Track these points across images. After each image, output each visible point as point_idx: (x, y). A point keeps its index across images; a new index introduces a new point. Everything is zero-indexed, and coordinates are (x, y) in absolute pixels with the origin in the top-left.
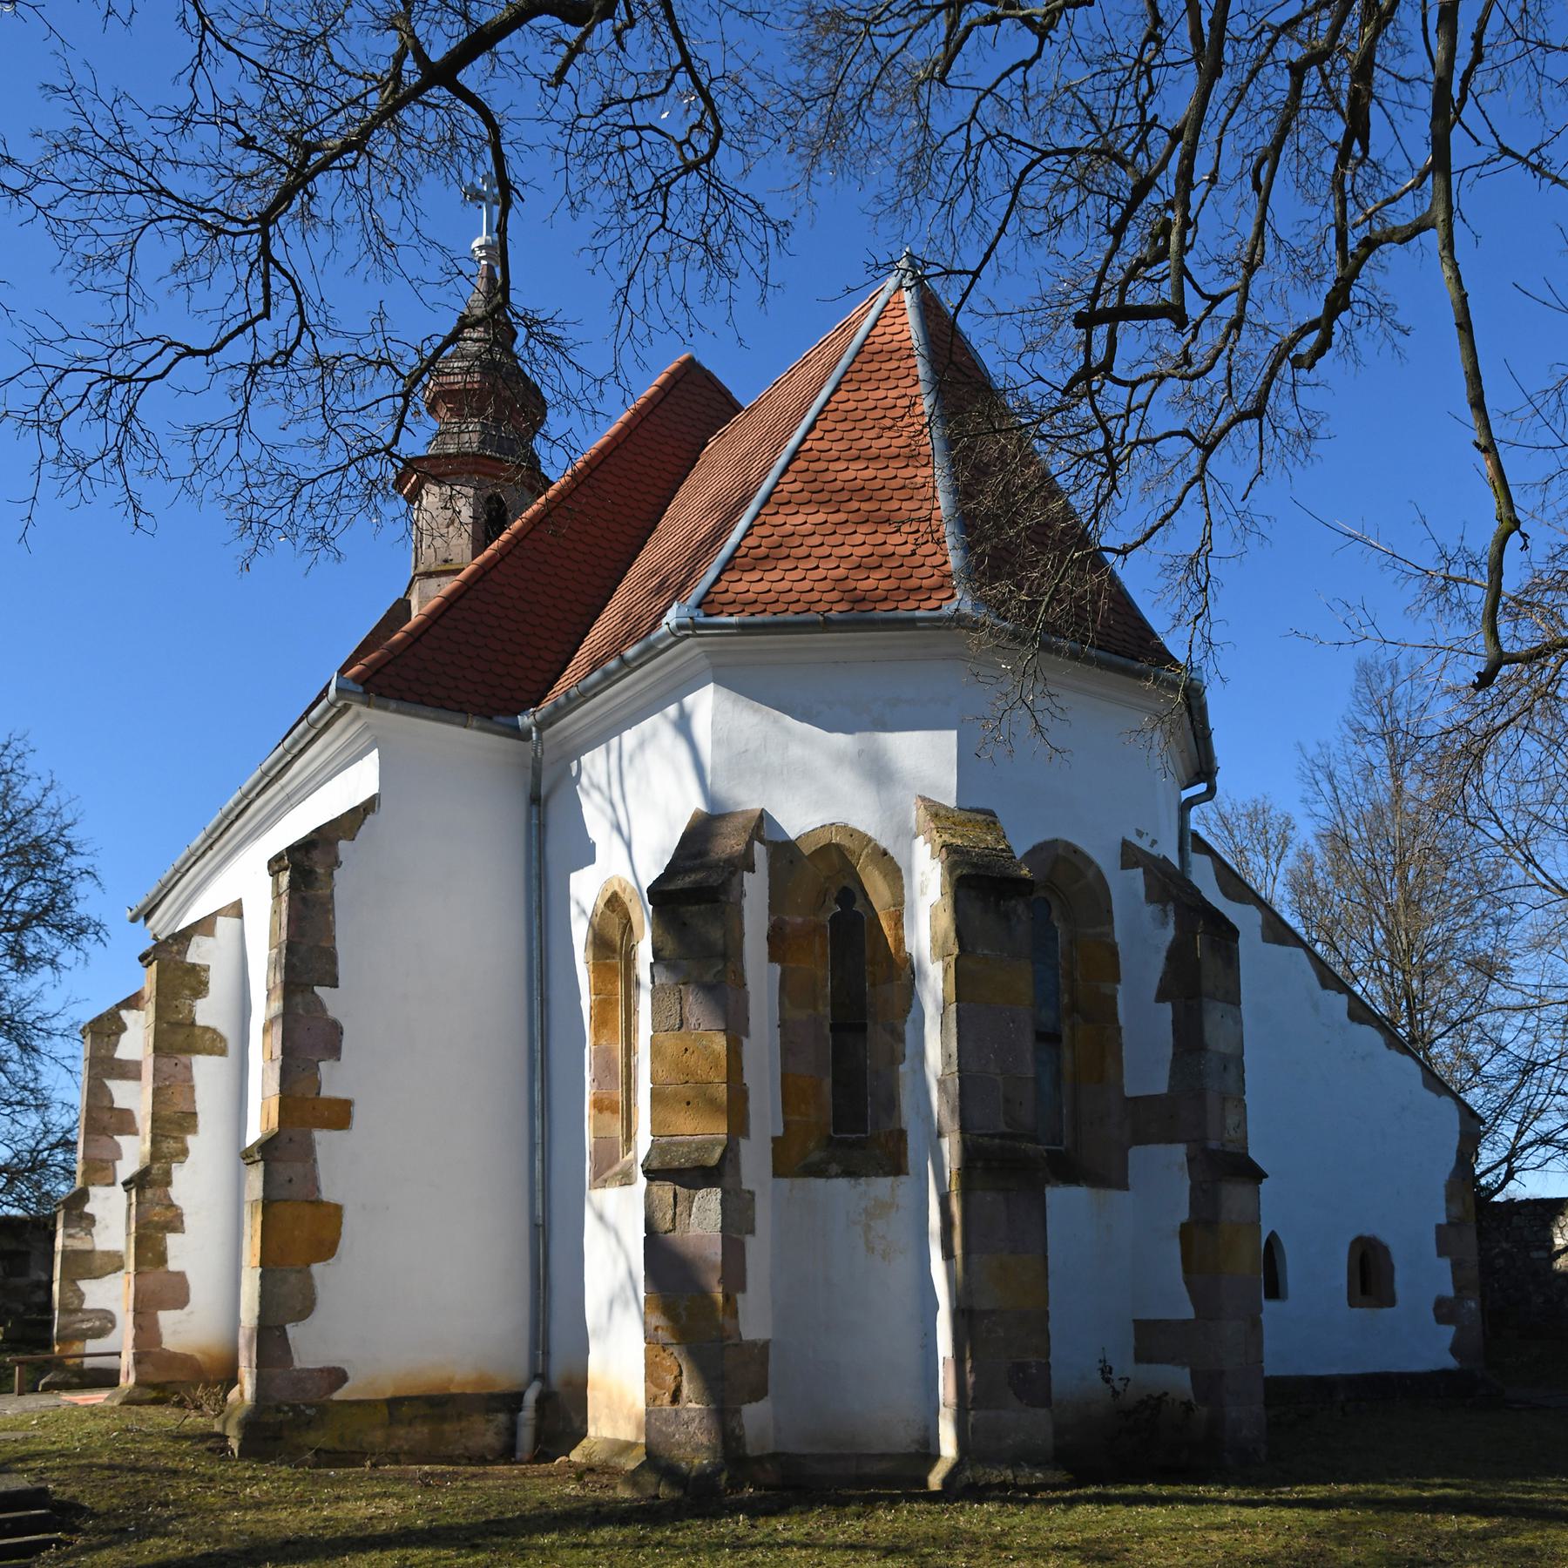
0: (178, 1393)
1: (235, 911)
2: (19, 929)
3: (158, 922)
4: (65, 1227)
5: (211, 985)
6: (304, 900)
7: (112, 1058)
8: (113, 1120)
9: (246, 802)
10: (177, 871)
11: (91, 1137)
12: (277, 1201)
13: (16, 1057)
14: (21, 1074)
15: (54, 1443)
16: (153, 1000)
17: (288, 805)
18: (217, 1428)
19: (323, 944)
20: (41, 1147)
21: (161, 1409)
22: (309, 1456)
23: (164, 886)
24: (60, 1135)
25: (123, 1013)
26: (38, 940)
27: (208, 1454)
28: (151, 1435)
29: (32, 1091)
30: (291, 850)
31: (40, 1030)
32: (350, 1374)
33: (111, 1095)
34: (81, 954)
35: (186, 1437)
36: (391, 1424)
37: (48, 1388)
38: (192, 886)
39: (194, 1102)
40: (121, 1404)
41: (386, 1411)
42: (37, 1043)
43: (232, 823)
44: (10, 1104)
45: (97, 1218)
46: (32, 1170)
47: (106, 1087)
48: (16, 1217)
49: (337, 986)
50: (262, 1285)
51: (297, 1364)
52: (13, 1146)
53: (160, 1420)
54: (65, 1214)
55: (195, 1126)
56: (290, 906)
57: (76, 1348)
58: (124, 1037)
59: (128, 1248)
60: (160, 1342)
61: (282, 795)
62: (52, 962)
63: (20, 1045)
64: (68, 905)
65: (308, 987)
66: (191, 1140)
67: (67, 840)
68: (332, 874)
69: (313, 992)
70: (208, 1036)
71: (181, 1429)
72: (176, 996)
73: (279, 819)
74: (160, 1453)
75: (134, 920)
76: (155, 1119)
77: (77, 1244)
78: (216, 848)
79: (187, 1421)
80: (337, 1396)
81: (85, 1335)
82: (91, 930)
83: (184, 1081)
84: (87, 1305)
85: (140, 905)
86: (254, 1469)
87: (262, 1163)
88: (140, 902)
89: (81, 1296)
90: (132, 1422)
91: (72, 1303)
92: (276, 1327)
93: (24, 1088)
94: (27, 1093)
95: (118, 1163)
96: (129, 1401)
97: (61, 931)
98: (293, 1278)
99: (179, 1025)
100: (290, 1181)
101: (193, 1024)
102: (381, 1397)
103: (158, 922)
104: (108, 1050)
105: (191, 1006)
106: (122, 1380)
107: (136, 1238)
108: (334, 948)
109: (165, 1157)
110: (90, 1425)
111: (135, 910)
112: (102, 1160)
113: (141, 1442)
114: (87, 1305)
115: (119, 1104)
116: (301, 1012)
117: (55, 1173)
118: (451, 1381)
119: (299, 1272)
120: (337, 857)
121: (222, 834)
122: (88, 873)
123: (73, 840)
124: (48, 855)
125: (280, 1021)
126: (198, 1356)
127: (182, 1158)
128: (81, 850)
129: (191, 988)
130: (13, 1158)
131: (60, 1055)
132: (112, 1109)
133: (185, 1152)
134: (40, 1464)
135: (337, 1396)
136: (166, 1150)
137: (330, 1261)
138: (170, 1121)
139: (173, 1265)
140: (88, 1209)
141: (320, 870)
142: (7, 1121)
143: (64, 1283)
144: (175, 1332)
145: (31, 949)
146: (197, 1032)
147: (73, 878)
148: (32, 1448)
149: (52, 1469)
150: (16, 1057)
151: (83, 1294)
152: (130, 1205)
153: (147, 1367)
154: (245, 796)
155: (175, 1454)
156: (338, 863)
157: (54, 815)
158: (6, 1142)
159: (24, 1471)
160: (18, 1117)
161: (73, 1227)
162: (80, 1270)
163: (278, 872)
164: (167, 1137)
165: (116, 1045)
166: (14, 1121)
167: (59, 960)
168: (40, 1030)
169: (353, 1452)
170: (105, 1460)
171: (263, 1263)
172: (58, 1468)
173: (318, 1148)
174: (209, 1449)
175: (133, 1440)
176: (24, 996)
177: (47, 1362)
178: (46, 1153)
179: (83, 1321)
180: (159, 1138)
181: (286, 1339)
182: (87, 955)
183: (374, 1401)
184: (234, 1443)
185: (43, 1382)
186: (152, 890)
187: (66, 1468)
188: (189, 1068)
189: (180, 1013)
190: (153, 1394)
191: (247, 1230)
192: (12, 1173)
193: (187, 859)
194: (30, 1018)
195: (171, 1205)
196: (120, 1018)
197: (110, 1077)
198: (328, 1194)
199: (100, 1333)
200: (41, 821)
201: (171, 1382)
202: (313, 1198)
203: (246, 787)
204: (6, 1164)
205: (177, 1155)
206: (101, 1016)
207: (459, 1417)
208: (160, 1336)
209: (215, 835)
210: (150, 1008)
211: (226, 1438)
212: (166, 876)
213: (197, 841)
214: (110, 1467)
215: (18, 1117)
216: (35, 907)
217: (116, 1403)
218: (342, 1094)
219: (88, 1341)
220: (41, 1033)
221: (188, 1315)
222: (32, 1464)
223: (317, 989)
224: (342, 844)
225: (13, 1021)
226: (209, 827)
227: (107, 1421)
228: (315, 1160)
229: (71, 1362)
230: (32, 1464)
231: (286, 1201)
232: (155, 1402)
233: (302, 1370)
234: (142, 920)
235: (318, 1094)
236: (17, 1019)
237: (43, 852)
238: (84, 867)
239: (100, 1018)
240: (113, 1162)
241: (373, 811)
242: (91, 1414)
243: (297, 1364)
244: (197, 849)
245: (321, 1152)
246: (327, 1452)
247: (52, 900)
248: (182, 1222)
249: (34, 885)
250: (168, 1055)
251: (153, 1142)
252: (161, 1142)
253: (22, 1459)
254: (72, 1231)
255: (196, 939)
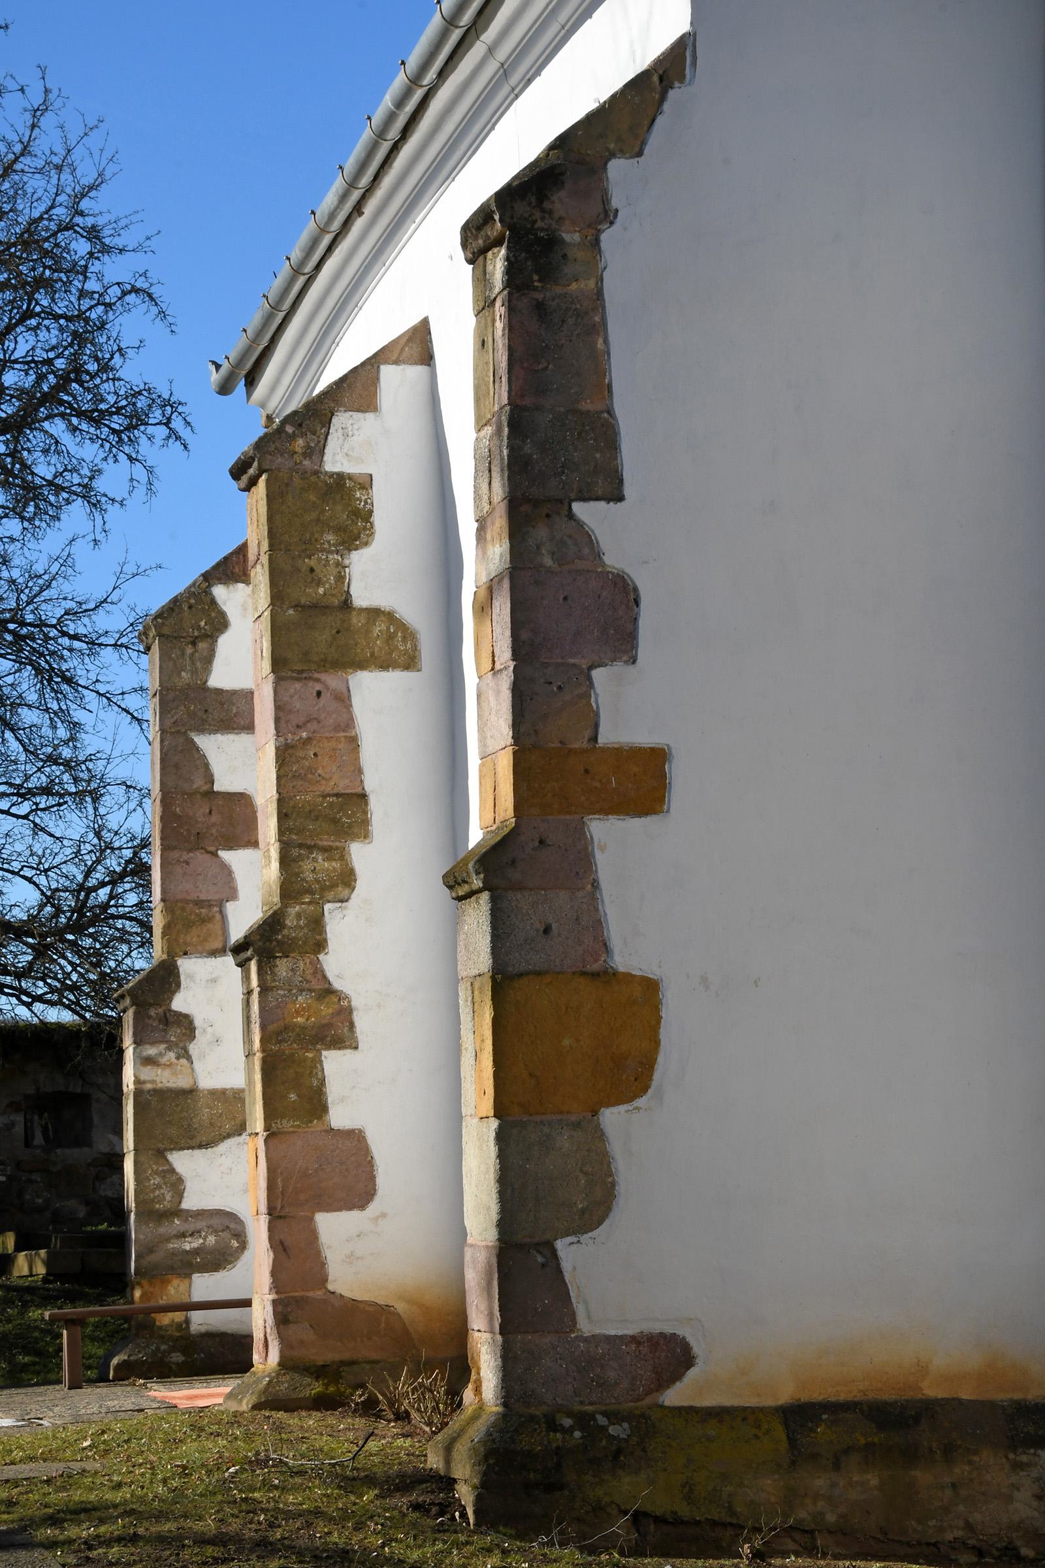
0: (362, 1386)
1: (415, 350)
2: (15, 426)
3: (273, 388)
4: (138, 1042)
5: (378, 519)
6: (540, 309)
7: (204, 688)
8: (215, 818)
9: (419, 94)
10: (297, 272)
11: (175, 854)
12: (521, 975)
13: (32, 697)
14: (46, 731)
15: (119, 1485)
16: (265, 559)
17: (506, 89)
18: (434, 1461)
19: (586, 406)
20: (92, 882)
21: (331, 1419)
22: (619, 1526)
23: (275, 308)
24: (128, 854)
25: (219, 592)
26: (54, 447)
27: (414, 1515)
28: (301, 1473)
29: (68, 765)
30: (507, 196)
31: (75, 637)
32: (697, 1349)
33: (207, 766)
34: (139, 471)
35: (370, 1480)
36: (793, 1463)
37: (126, 1373)
38: (330, 303)
39: (360, 771)
40: (257, 1407)
41: (780, 1433)
42: (71, 664)
43: (395, 148)
44: (24, 794)
45: (198, 1022)
46: (78, 928)
47: (197, 749)
48: (59, 1026)
49: (620, 498)
50: (502, 1156)
51: (585, 1327)
52: (42, 880)
53: (323, 1441)
54: (136, 1014)
55: (365, 822)
56: (511, 328)
57: (174, 1291)
58: (225, 643)
59: (250, 1081)
60: (322, 1279)
61: (492, 67)
62: (87, 493)
63: (38, 671)
64: (105, 367)
65: (560, 507)
66: (359, 853)
67: (89, 221)
68: (596, 243)
69: (571, 515)
70: (379, 627)
71: (361, 1461)
72: (309, 547)
73: (490, 126)
74: (317, 1513)
75: (225, 389)
76: (283, 803)
77: (164, 1079)
78: (369, 209)
79: (372, 1445)
80: (673, 1396)
81: (189, 1265)
82: (156, 415)
83: (337, 728)
84: (190, 1203)
85: (233, 356)
86: (505, 1552)
87: (485, 896)
88: (233, 347)
89: (177, 1185)
90: (266, 1443)
91: (160, 1200)
92: (538, 1246)
93: (53, 760)
94: (57, 770)
95: (230, 907)
96: (270, 1402)
97: (97, 423)
98: (564, 1141)
99: (318, 608)
100: (547, 930)
101: (346, 604)
102: (769, 1402)
103: (273, 388)
104: (194, 672)
105: (341, 566)
106: (256, 1358)
107: (264, 1061)
108: (610, 411)
109: (310, 891)
110: (190, 1450)
111: (226, 366)
112: (199, 903)
113: (283, 1489)
114: (190, 1203)
115: (223, 784)
116: (548, 561)
117: (123, 930)
118: (922, 1369)
119: (576, 1125)
120: (605, 200)
121: (377, 178)
122: (135, 290)
123: (101, 221)
124: (57, 259)
125: (506, 584)
126: (401, 1307)
127: (343, 892)
128: (119, 242)
129: (339, 529)
130: (41, 907)
131: (115, 688)
132: (211, 794)
133: (347, 878)
134: (85, 1531)
135: (673, 1396)
136: (310, 877)
137: (641, 1102)
138: (313, 814)
139: (339, 1117)
140: (179, 1003)
141: (571, 237)
142: (22, 828)
143: (142, 1159)
144: (351, 1258)
145: (44, 470)
146: (357, 621)
147: (109, 306)
148: (78, 1495)
149: (108, 1543)
150: (32, 697)
151: (180, 1180)
152: (249, 993)
153: (301, 1331)
154: (415, 81)
155: (345, 1515)
156: (608, 216)
157: (59, 168)
158: (28, 873)
159: (52, 1545)
160: (46, 820)
161: (153, 1043)
162: (173, 1131)
163: (484, 251)
164: (310, 848)
165: (209, 658)
166: (37, 828)
167: (100, 485)
168: (75, 637)
169: (714, 1524)
170: (209, 1525)
171: (500, 1111)
172: (119, 1540)
173: (600, 858)
174: (416, 1507)
175: (267, 1485)
176: (39, 568)
177: (127, 1317)
178: (103, 893)
179: (183, 1235)
180: (295, 852)
181: (559, 1271)
182: (150, 471)
183: (753, 1410)
184: (465, 1494)
185: (115, 1361)
186: (254, 321)
187: (134, 1539)
188: (344, 699)
189: (319, 583)
190: (317, 1388)
191: (468, 1040)
192: (43, 936)
193: (315, 242)
194: (51, 613)
195: (328, 992)
196: (213, 602)
197: (201, 730)
198: (624, 959)
199: (218, 1260)
200: (35, 183)
201: (352, 1363)
202: (596, 967)
203: (413, 61)
204: (32, 918)
205: (333, 886)
206: (175, 600)
207: (949, 1451)
208: (323, 1265)
209: (365, 181)
210: (260, 575)
211: (449, 1483)
212: (278, 283)
213: (330, 199)
214: (219, 1540)
215: (46, 820)
216: (41, 378)
217: (245, 1406)
218: (643, 737)
219: (196, 1277)
220: (77, 644)
221: (375, 1220)
222: (72, 1532)
223: (577, 507)
224: (617, 168)
225: (23, 624)
226: (350, 164)
227: (222, 1442)
228: (595, 884)
229: (165, 1319)
230: (72, 1532)
231: (539, 974)
232: (323, 1403)
233: (595, 1339)
234: (241, 386)
235: (594, 739)
236: (29, 618)
237: (46, 253)
238: (126, 277)
239: (175, 605)
240: (221, 904)
241: (682, 78)
242: (193, 1426)
243: (585, 1327)
244: (332, 216)
245: (605, 865)
246: (659, 1520)
247: (74, 359)
248: (352, 1026)
249: (35, 329)
250: (302, 676)
251: (285, 861)
252: (300, 858)
253: (54, 1520)
254: (151, 1051)
255: (341, 420)
